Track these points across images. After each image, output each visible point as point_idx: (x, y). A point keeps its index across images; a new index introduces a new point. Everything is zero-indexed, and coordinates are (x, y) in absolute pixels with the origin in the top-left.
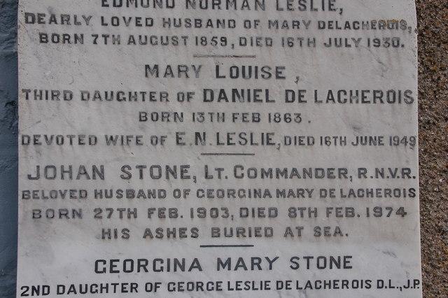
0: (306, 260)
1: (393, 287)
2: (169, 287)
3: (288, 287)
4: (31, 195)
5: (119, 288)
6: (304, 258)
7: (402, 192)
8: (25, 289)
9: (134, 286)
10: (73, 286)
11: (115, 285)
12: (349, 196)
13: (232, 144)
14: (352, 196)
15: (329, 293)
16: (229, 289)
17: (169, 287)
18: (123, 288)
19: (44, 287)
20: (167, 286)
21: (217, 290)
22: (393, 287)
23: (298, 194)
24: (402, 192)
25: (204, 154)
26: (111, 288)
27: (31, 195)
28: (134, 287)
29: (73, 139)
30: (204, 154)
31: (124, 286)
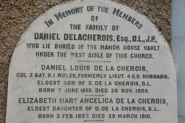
0: (49, 99)
1: (149, 85)
2: (139, 101)
3: (77, 91)
4: (43, 101)
5: (75, 108)
6: (48, 99)
7: (133, 83)
8: (113, 90)
9: (81, 108)
10: (58, 107)
11: (73, 107)
12: (35, 103)
13: (124, 85)
14: (36, 102)
15: (99, 122)
16: (110, 77)
17: (139, 101)
18: (76, 109)
19: (45, 53)
20: (138, 100)
21: (95, 102)
22: (149, 85)
23: (161, 77)
24: (133, 83)
25: (162, 77)
26: (72, 109)
27: (43, 101)
28: (71, 116)
29: (51, 100)
30: (162, 77)
31: (29, 108)
